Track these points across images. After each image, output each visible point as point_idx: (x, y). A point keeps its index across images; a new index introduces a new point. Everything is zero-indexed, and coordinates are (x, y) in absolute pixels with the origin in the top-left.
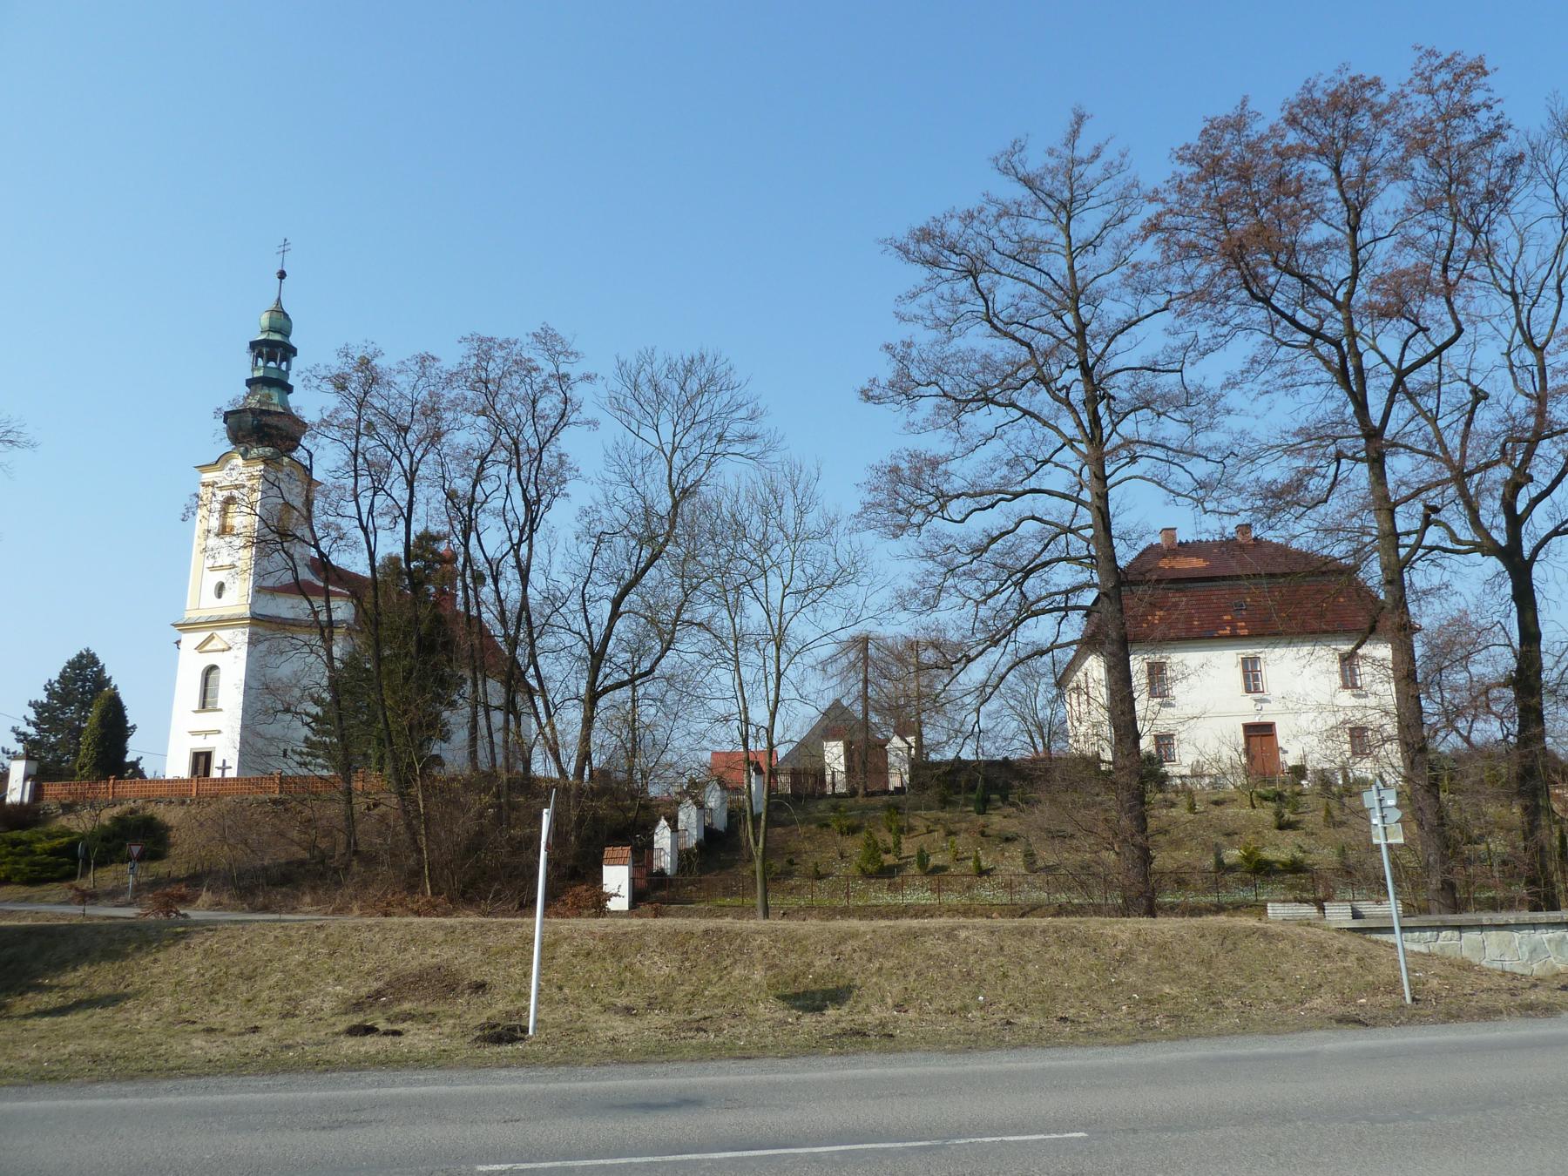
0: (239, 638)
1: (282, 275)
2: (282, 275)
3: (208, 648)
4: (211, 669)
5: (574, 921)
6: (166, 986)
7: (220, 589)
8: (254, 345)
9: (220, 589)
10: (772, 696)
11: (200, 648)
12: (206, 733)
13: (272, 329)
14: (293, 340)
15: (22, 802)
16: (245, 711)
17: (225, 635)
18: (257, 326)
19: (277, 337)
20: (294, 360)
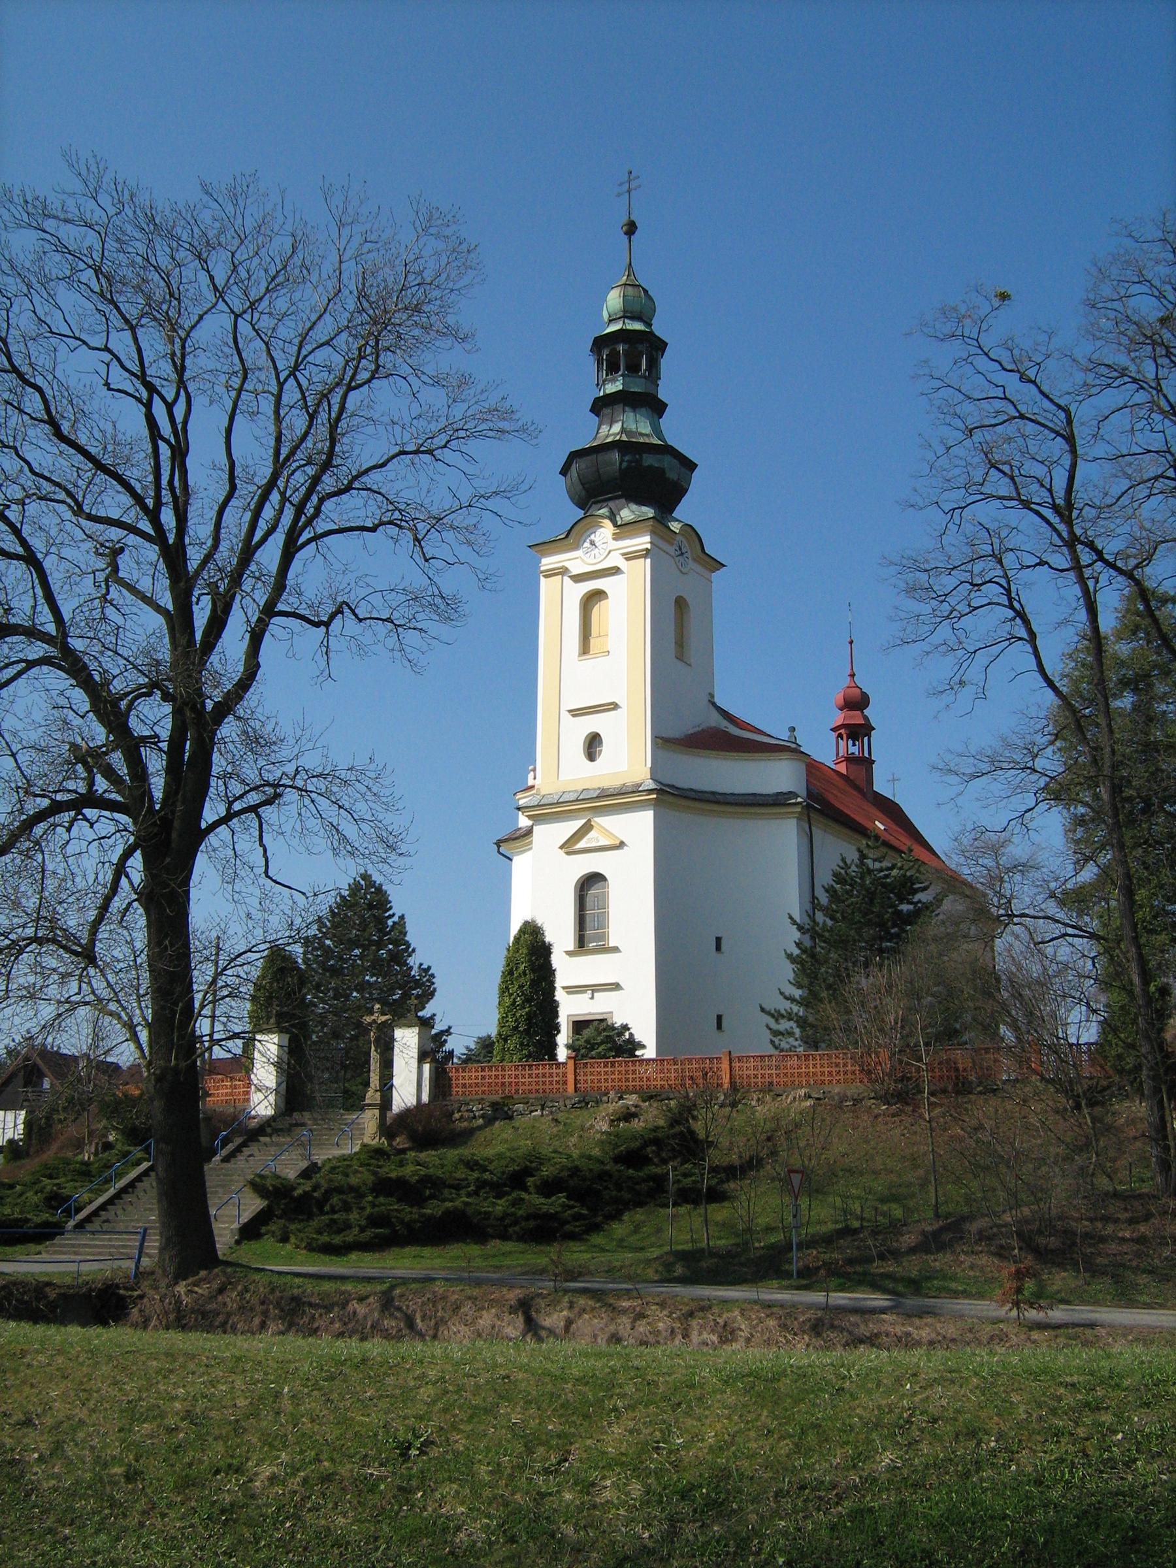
0: (638, 828)
1: (631, 229)
2: (631, 229)
3: (582, 844)
4: (591, 882)
5: (94, 1331)
6: (636, 1334)
7: (593, 745)
8: (600, 343)
9: (593, 745)
10: (263, 335)
11: (569, 846)
12: (595, 989)
13: (628, 313)
14: (658, 329)
15: (419, 1105)
16: (738, 751)
17: (611, 825)
18: (625, 220)
19: (638, 326)
20: (666, 363)
